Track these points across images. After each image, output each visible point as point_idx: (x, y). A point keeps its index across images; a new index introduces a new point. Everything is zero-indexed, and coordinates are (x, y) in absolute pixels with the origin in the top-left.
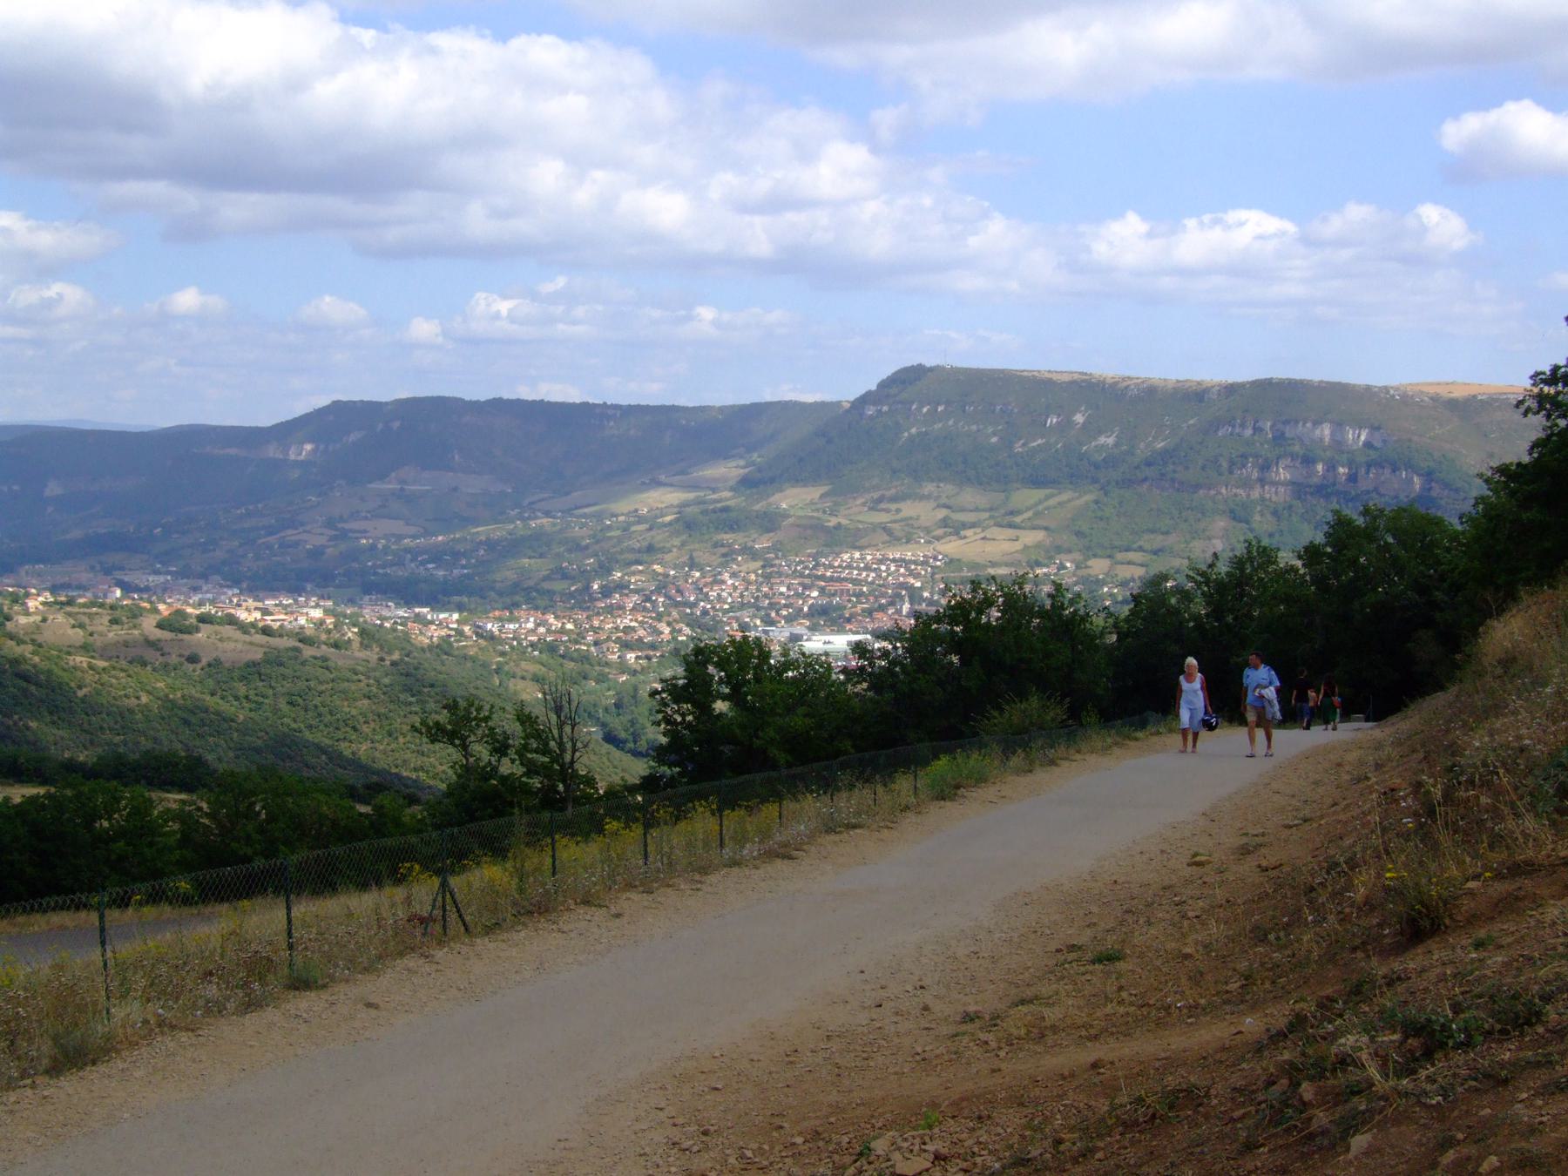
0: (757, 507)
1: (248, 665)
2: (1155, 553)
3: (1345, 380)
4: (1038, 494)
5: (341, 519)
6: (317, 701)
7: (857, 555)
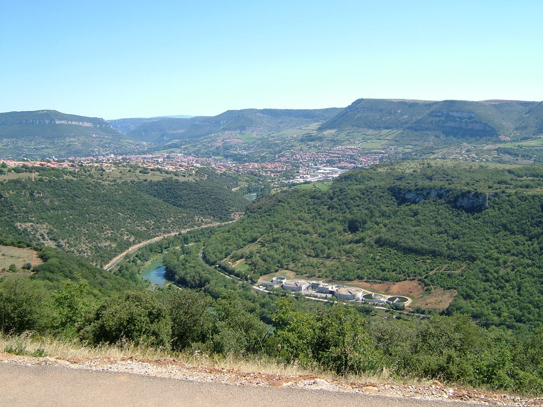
0: (320, 135)
1: (158, 182)
2: (415, 146)
3: (466, 100)
4: (388, 131)
5: (225, 139)
6: (173, 191)
7: (340, 147)
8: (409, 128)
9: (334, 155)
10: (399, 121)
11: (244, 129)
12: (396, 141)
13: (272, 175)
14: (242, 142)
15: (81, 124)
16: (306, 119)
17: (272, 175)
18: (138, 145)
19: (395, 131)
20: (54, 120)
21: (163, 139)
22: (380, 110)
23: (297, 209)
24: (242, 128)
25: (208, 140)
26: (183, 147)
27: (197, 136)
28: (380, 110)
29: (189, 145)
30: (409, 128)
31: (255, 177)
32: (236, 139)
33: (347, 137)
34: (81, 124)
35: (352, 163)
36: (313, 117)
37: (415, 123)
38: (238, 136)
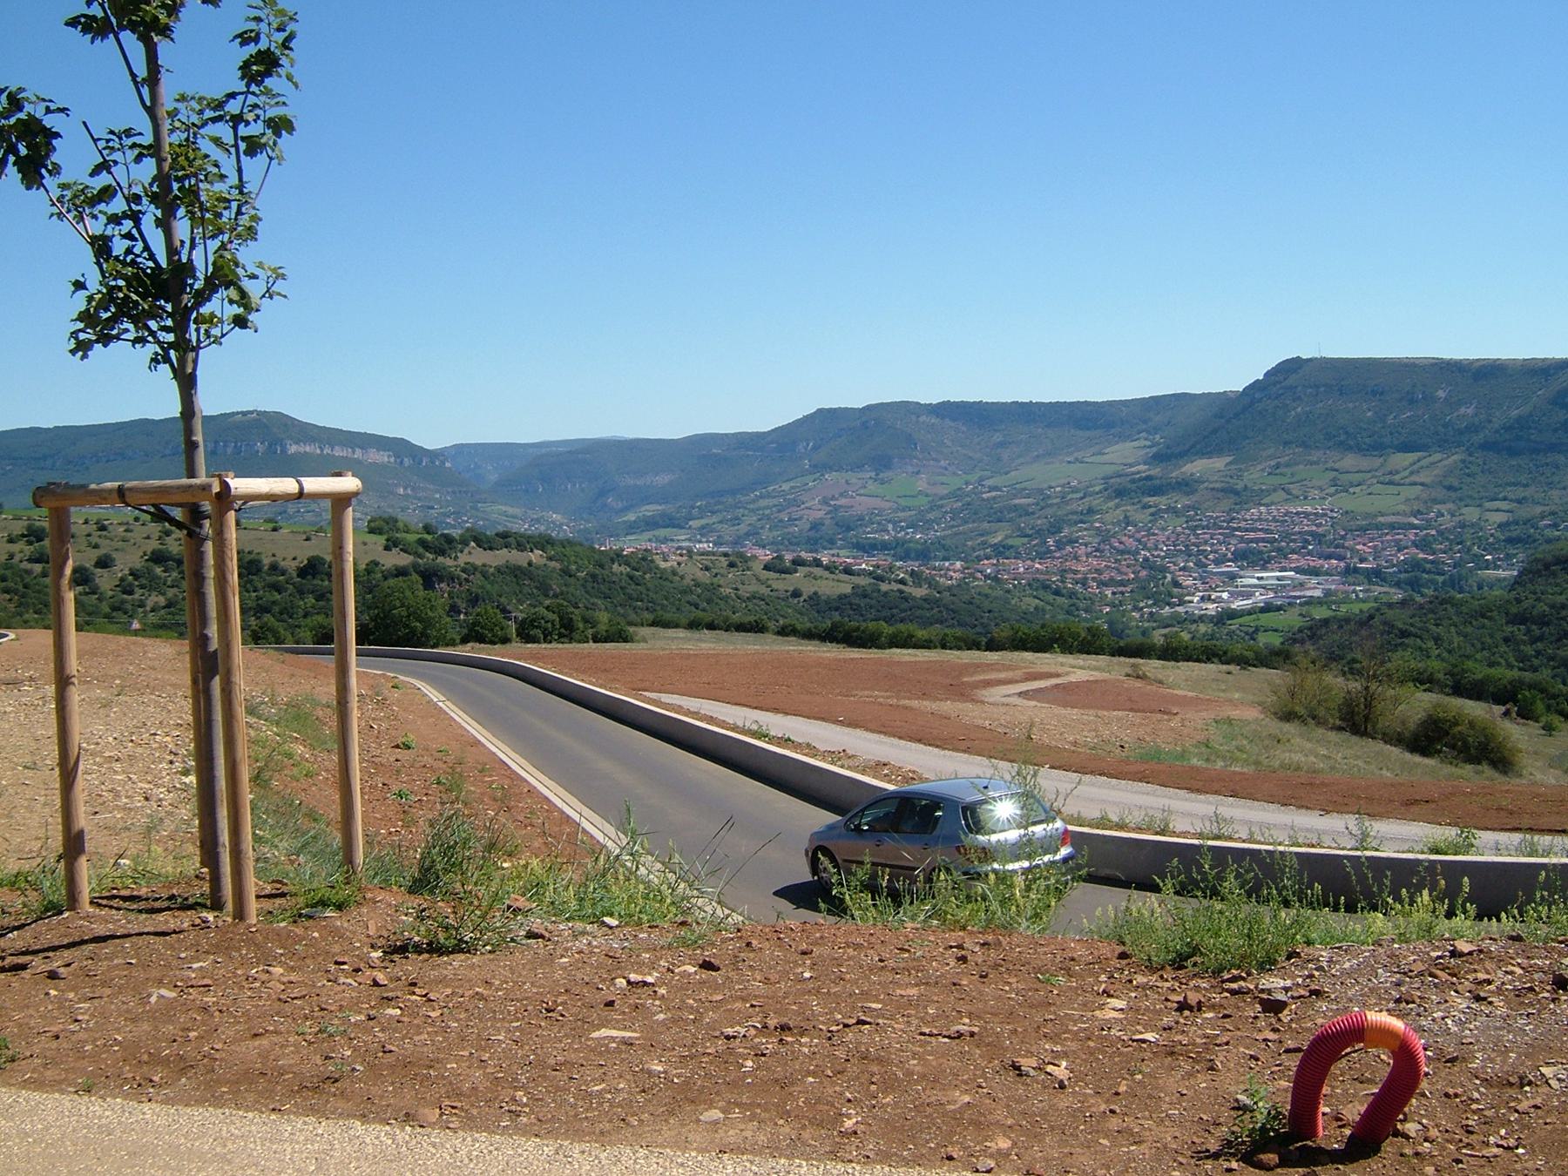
2: (1519, 502)
4: (1411, 457)
5: (833, 498)
8: (1486, 446)
9: (1252, 535)
10: (1445, 426)
11: (888, 466)
12: (1450, 488)
13: (1109, 593)
14: (888, 505)
15: (358, 454)
16: (1088, 433)
17: (1109, 593)
18: (538, 521)
19: (1437, 456)
20: (281, 442)
21: (605, 505)
22: (1374, 393)
23: (1478, 656)
24: (882, 463)
25: (775, 501)
26: (694, 524)
27: (733, 492)
28: (1374, 393)
29: (714, 519)
30: (1486, 446)
31: (1060, 600)
32: (864, 495)
33: (1276, 480)
34: (358, 454)
35: (1329, 557)
36: (1109, 425)
37: (1508, 429)
38: (872, 487)
